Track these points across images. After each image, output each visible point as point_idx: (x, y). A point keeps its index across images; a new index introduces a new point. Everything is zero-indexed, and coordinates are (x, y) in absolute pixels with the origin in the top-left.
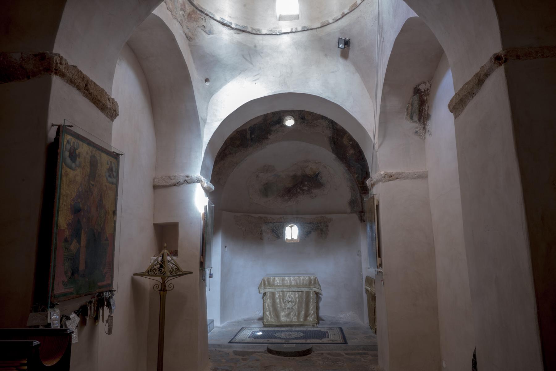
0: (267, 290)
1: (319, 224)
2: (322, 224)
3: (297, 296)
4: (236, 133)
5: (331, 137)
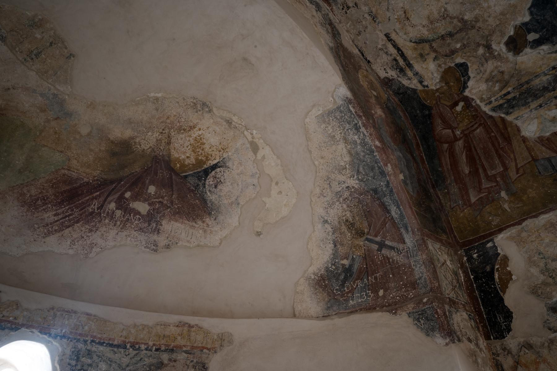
1: (165, 357)
2: (181, 357)
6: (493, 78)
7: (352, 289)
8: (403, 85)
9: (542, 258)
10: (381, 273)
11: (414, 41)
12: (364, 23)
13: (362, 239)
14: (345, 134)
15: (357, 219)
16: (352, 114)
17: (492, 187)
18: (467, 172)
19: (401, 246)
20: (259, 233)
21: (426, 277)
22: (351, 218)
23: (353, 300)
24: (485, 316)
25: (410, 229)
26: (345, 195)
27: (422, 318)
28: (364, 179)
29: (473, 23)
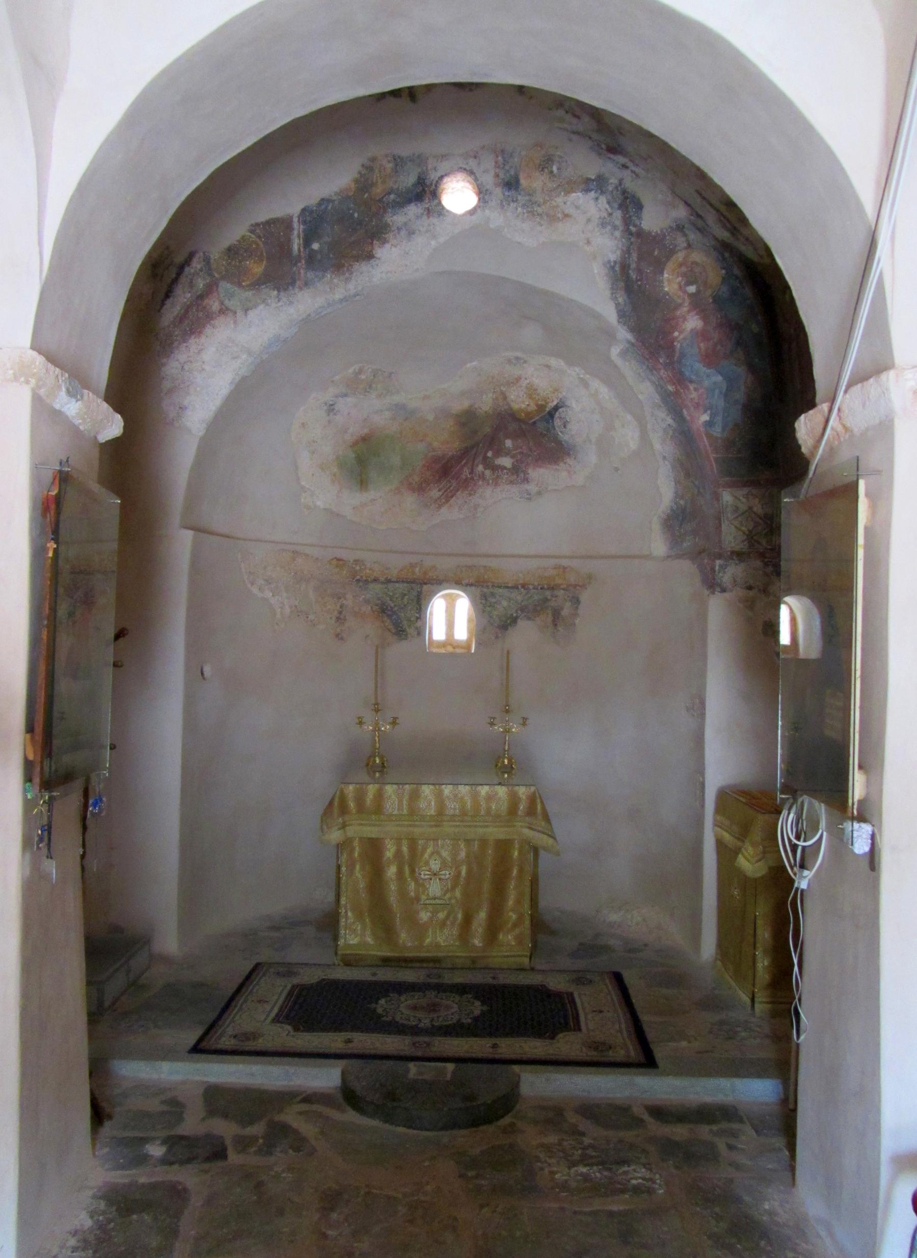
0: (351, 831)
1: (548, 594)
3: (463, 854)
4: (252, 231)
5: (615, 262)
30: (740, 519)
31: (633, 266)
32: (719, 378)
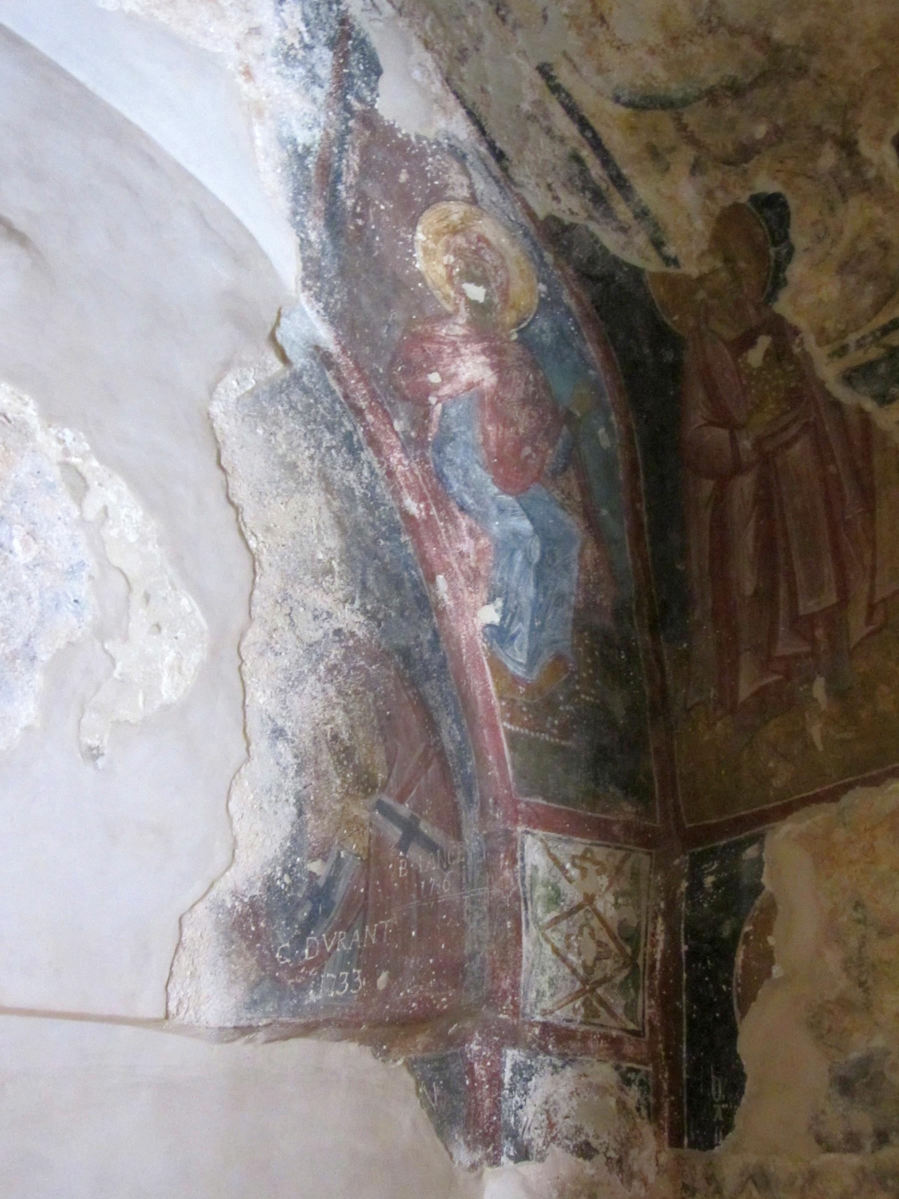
5: (308, 150)
6: (860, 261)
7: (320, 956)
8: (606, 251)
9: (859, 922)
10: (394, 920)
11: (625, 98)
12: (470, 20)
13: (368, 800)
14: (322, 461)
15: (361, 735)
16: (335, 400)
17: (797, 657)
18: (749, 588)
19: (452, 845)
20: (95, 752)
21: (487, 956)
22: (347, 731)
23: (316, 989)
24: (685, 1076)
25: (477, 795)
26: (332, 657)
27: (439, 1080)
28: (378, 612)
29: (802, 55)
30: (563, 925)
31: (349, 178)
32: (525, 526)
